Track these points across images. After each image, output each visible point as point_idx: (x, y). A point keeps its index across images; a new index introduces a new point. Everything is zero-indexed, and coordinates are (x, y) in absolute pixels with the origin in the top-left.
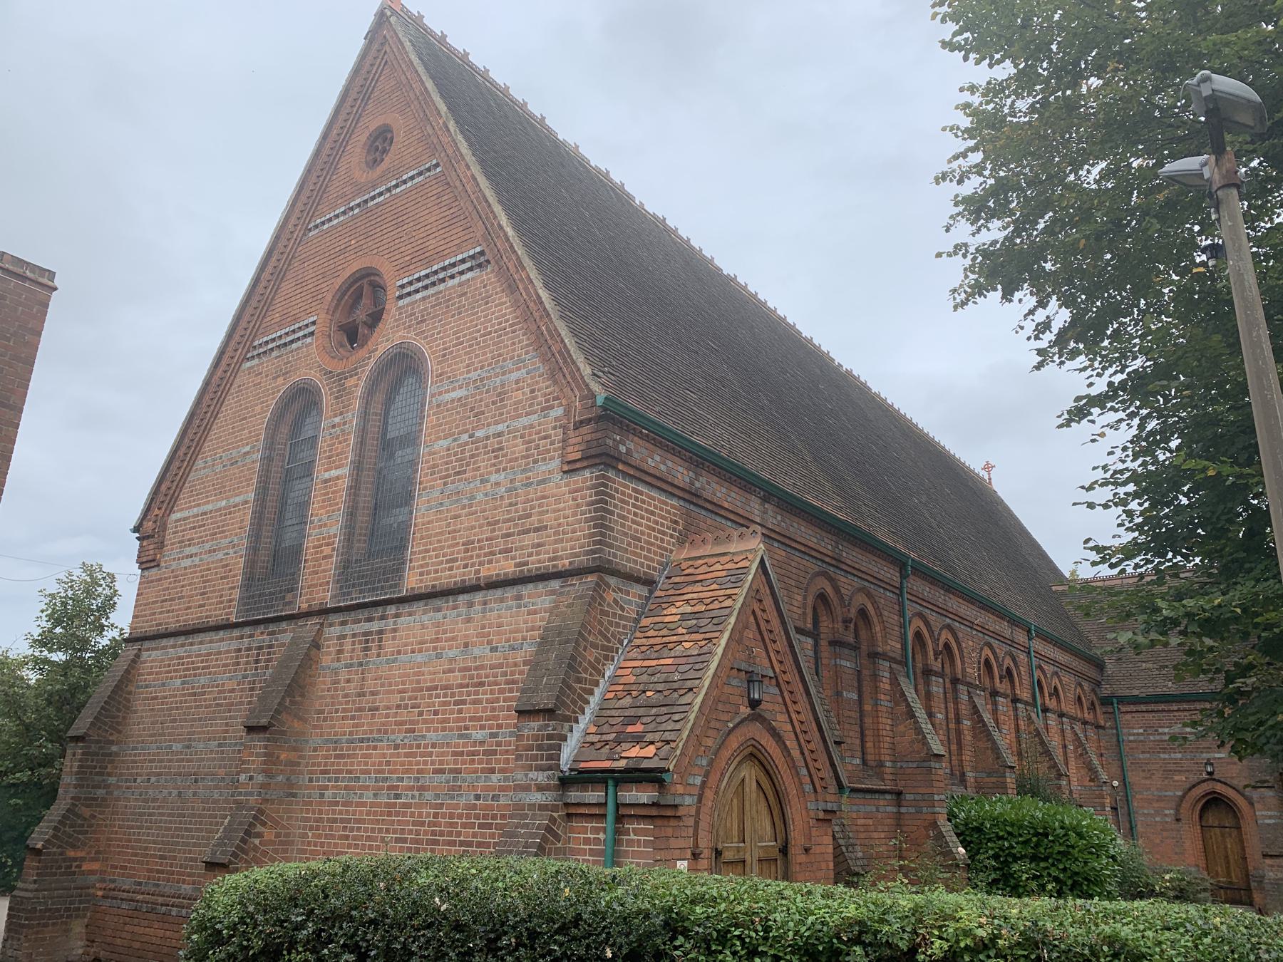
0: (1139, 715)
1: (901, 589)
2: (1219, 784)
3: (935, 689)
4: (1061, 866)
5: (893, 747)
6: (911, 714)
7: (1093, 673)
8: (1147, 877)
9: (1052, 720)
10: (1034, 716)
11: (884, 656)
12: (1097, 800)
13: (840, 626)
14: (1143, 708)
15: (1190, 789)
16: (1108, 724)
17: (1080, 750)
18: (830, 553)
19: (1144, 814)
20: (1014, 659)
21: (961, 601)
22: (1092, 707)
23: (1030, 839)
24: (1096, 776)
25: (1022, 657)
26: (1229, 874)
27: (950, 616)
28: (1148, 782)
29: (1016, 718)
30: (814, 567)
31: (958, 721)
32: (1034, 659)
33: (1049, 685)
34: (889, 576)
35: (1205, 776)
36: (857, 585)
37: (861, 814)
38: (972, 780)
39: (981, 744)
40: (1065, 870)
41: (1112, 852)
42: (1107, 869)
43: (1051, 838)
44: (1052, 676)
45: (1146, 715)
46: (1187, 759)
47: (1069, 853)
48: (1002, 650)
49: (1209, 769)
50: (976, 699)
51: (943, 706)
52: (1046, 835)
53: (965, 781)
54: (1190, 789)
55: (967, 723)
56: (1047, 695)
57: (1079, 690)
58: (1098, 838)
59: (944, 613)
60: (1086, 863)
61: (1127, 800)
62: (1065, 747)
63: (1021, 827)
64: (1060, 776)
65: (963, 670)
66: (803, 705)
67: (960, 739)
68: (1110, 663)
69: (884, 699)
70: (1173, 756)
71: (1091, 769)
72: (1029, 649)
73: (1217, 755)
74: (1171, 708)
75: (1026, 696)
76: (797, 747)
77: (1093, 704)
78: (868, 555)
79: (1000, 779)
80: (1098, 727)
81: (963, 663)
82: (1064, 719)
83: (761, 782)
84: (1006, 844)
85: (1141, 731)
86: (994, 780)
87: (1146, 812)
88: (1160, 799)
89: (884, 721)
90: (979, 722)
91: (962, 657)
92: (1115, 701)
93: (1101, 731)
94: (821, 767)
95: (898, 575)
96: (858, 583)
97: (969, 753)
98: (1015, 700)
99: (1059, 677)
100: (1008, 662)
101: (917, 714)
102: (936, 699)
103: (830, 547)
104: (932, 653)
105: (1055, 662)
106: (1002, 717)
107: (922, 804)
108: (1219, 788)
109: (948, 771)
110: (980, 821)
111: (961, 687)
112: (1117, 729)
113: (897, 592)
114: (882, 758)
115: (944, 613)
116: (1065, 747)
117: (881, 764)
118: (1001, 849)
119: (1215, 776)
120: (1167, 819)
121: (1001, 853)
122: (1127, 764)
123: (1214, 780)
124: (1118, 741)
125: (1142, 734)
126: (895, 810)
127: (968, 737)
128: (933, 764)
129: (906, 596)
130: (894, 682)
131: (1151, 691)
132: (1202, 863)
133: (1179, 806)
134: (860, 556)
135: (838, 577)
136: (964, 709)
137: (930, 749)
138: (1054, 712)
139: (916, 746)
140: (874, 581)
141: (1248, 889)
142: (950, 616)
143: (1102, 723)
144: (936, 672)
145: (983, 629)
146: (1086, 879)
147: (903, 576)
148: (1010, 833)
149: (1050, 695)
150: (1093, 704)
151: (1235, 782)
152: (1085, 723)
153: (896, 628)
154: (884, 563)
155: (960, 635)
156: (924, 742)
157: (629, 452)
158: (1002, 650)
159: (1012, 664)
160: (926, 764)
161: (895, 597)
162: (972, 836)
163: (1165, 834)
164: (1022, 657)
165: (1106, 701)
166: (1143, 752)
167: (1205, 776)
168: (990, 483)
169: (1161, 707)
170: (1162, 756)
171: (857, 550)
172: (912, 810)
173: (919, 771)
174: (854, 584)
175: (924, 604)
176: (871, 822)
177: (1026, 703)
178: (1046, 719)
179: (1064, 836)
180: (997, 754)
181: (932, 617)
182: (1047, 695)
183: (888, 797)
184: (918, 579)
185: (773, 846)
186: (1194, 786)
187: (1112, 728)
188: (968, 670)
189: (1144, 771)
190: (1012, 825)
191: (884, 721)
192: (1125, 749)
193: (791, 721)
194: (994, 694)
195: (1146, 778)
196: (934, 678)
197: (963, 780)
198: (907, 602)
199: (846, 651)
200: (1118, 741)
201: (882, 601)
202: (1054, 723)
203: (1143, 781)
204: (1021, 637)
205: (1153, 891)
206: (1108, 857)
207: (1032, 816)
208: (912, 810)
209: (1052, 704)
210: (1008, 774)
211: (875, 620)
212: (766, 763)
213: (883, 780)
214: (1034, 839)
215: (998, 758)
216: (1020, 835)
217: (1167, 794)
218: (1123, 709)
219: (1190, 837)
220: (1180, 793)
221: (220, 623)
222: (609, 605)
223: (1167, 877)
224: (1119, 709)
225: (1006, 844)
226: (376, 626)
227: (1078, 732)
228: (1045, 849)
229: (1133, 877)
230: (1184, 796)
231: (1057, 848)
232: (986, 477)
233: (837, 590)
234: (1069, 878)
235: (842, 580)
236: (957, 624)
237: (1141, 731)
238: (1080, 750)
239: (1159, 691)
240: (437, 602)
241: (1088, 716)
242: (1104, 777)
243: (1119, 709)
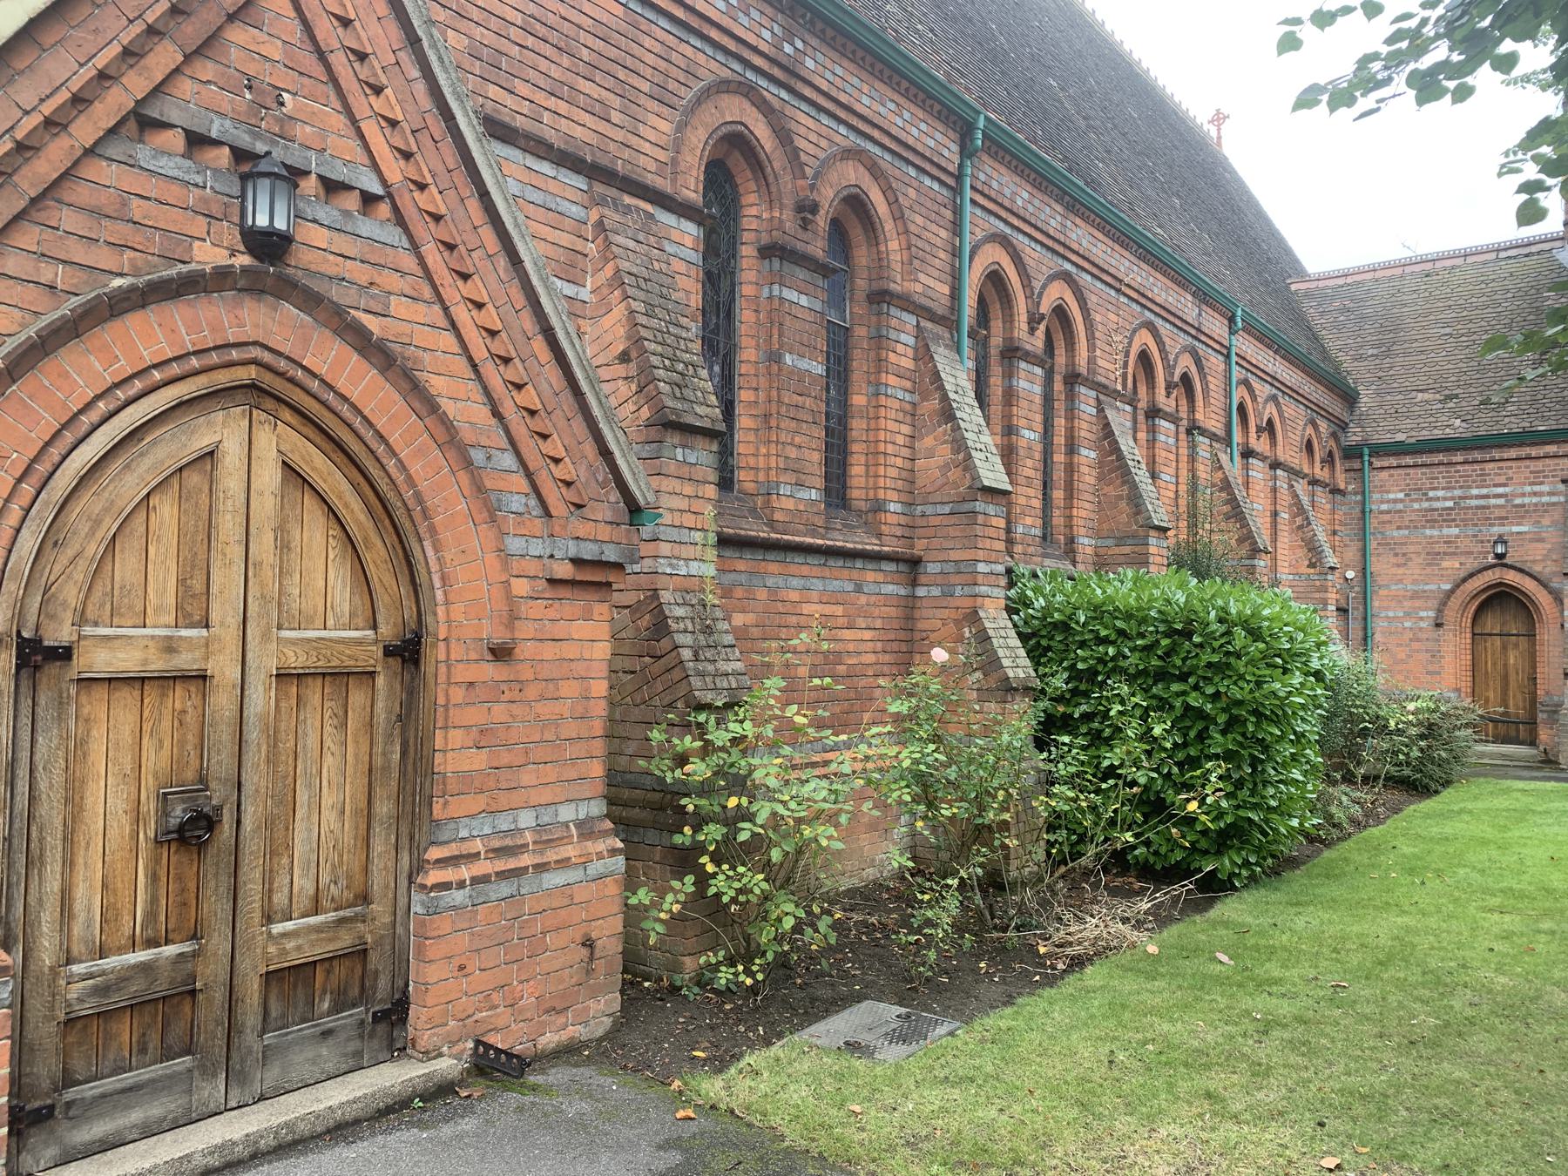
0: (1400, 471)
1: (959, 178)
2: (1512, 572)
3: (1023, 384)
4: (1210, 690)
5: (910, 475)
6: (948, 414)
7: (1337, 408)
8: (1378, 706)
9: (1258, 470)
10: (1224, 458)
11: (907, 303)
12: (1317, 595)
14: (1409, 460)
15: (1464, 580)
16: (1350, 488)
17: (1299, 520)
18: (764, 47)
19: (1388, 614)
20: (1198, 362)
21: (1100, 236)
22: (1329, 460)
23: (1158, 641)
24: (1320, 560)
25: (1215, 362)
26: (1504, 703)
27: (1074, 258)
28: (1401, 571)
29: (1192, 458)
30: (712, 67)
31: (1071, 449)
32: (1235, 368)
33: (1259, 415)
34: (932, 143)
35: (1491, 560)
36: (844, 143)
37: (814, 596)
38: (1089, 550)
39: (1110, 491)
40: (1216, 696)
41: (1315, 664)
42: (1300, 694)
43: (1197, 639)
44: (1266, 401)
45: (1411, 471)
46: (1467, 536)
47: (1228, 665)
48: (1175, 341)
49: (1500, 549)
50: (1110, 414)
51: (1039, 418)
52: (1188, 634)
53: (1073, 551)
54: (1464, 580)
55: (1088, 455)
56: (1253, 429)
57: (1310, 430)
58: (1291, 640)
59: (1061, 250)
60: (1259, 684)
61: (1365, 598)
62: (1275, 514)
63: (1144, 621)
64: (1255, 551)
65: (1091, 360)
66: (492, 280)
67: (1072, 480)
68: (1366, 400)
69: (896, 389)
70: (1446, 531)
71: (1313, 548)
72: (1229, 349)
73: (1515, 529)
74: (1454, 459)
75: (1214, 424)
76: (481, 398)
77: (1330, 454)
78: (878, 84)
79: (1136, 549)
80: (1335, 491)
81: (1092, 347)
82: (1279, 472)
83: (305, 469)
84: (1111, 651)
85: (1401, 496)
86: (1127, 550)
87: (1391, 614)
88: (1415, 596)
89: (892, 425)
90: (1111, 454)
91: (1091, 337)
92: (1366, 451)
93: (1338, 497)
94: (561, 453)
95: (955, 148)
96: (844, 137)
97: (1087, 505)
98: (1193, 429)
99: (1278, 405)
100: (1185, 363)
101: (958, 414)
102: (1023, 403)
103: (766, 34)
104: (1024, 318)
105: (1273, 380)
106: (1164, 454)
107: (954, 579)
108: (1512, 577)
109: (1038, 532)
110: (1068, 611)
111: (1083, 390)
112: (1363, 493)
113: (951, 181)
114: (881, 494)
115: (1061, 250)
116: (1275, 514)
117: (878, 507)
118: (1101, 661)
119: (1507, 561)
120: (1423, 624)
121: (1100, 668)
122: (1372, 544)
123: (1506, 565)
124: (1363, 512)
125: (1401, 501)
126: (903, 592)
127: (1087, 477)
128: (979, 506)
129: (968, 193)
130: (923, 354)
131: (1425, 434)
132: (1466, 685)
133: (1444, 603)
134: (855, 81)
135: (789, 111)
136: (1086, 429)
137: (976, 477)
138: (1264, 459)
139: (954, 474)
140: (893, 146)
141: (1532, 723)
142: (1074, 258)
143: (1342, 486)
144: (1027, 353)
145: (1142, 299)
146: (1256, 713)
147: (966, 151)
148: (1121, 633)
149: (1259, 430)
150: (1330, 454)
151: (1537, 568)
152: (1314, 482)
153: (942, 255)
154: (921, 114)
155: (1092, 300)
156: (967, 465)
158: (1175, 341)
159: (1193, 369)
160: (967, 507)
161: (945, 192)
162: (1052, 638)
163: (1416, 645)
164: (1215, 362)
165: (1352, 453)
166: (1399, 528)
167: (1491, 560)
168: (1219, 143)
169: (1441, 457)
170: (1428, 532)
171: (846, 63)
172: (936, 591)
173: (954, 520)
174: (838, 139)
175: (1016, 222)
176: (839, 610)
177: (1213, 437)
178: (1246, 468)
179: (1222, 635)
180: (1137, 506)
181: (1032, 253)
182: (1253, 429)
183: (891, 567)
184: (1003, 170)
185: (359, 642)
186: (1471, 575)
187: (1356, 493)
188: (1100, 362)
189: (1396, 555)
190: (1128, 616)
191: (892, 425)
192: (1372, 523)
193: (454, 326)
194: (1153, 413)
195: (1398, 566)
196: (1023, 365)
197: (1070, 552)
198: (968, 207)
199: (802, 274)
200: (1363, 512)
201: (912, 193)
202: (1260, 476)
203: (1395, 570)
204: (1215, 326)
205: (1386, 727)
206: (1307, 674)
207: (1168, 601)
208: (936, 591)
209: (1261, 445)
210: (1152, 541)
211: (889, 226)
212: (329, 421)
213: (879, 535)
214: (1165, 642)
215: (1138, 513)
216: (1142, 635)
217: (1426, 588)
218: (1377, 463)
219: (1455, 647)
220: (1448, 587)
223: (1411, 706)
224: (1371, 463)
225: (1111, 651)
227: (1300, 492)
228: (1184, 660)
229: (1357, 707)
230: (1452, 591)
231: (1207, 657)
232: (1214, 133)
233: (784, 136)
234: (1224, 710)
235: (804, 121)
236: (1089, 278)
237: (1401, 496)
238: (1299, 520)
239: (1438, 433)
241: (1320, 473)
242: (1332, 560)
243: (1371, 463)
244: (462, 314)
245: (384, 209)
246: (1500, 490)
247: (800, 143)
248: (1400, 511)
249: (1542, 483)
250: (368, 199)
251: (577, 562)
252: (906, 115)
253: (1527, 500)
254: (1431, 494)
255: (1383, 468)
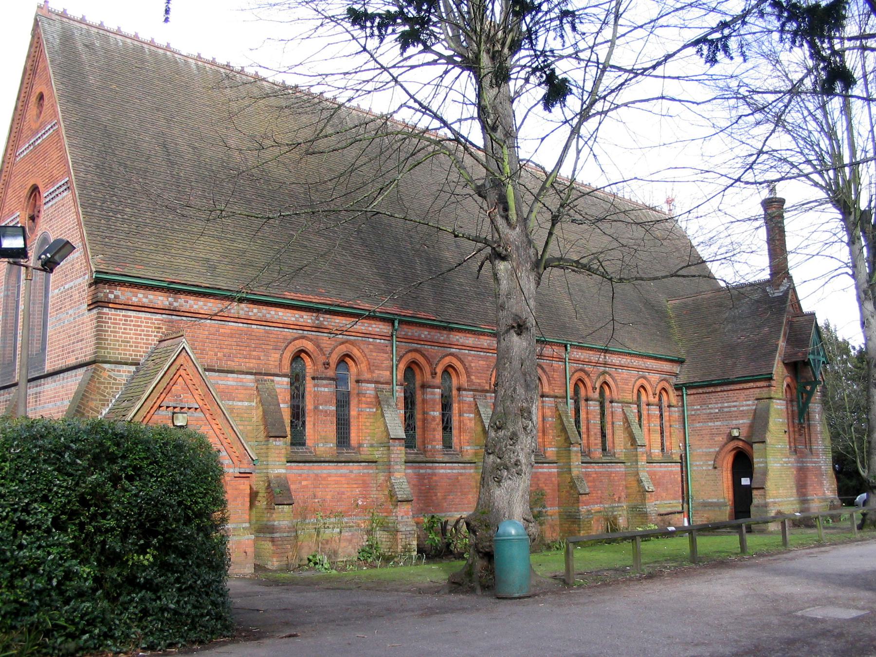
13: (321, 368)
45: (702, 396)
85: (699, 407)
157: (116, 297)
161: (386, 342)
163: (708, 478)
170: (710, 424)
195: (699, 440)
218: (689, 392)
220: (717, 449)
221: (56, 370)
222: (105, 379)
226: (38, 389)
237: (699, 407)
240: (55, 377)
244: (215, 427)
245: (199, 410)
246: (735, 404)
247: (323, 345)
248: (698, 414)
249: (749, 400)
250: (196, 409)
251: (240, 473)
252: (366, 325)
253: (745, 408)
254: (710, 406)
255: (691, 394)
